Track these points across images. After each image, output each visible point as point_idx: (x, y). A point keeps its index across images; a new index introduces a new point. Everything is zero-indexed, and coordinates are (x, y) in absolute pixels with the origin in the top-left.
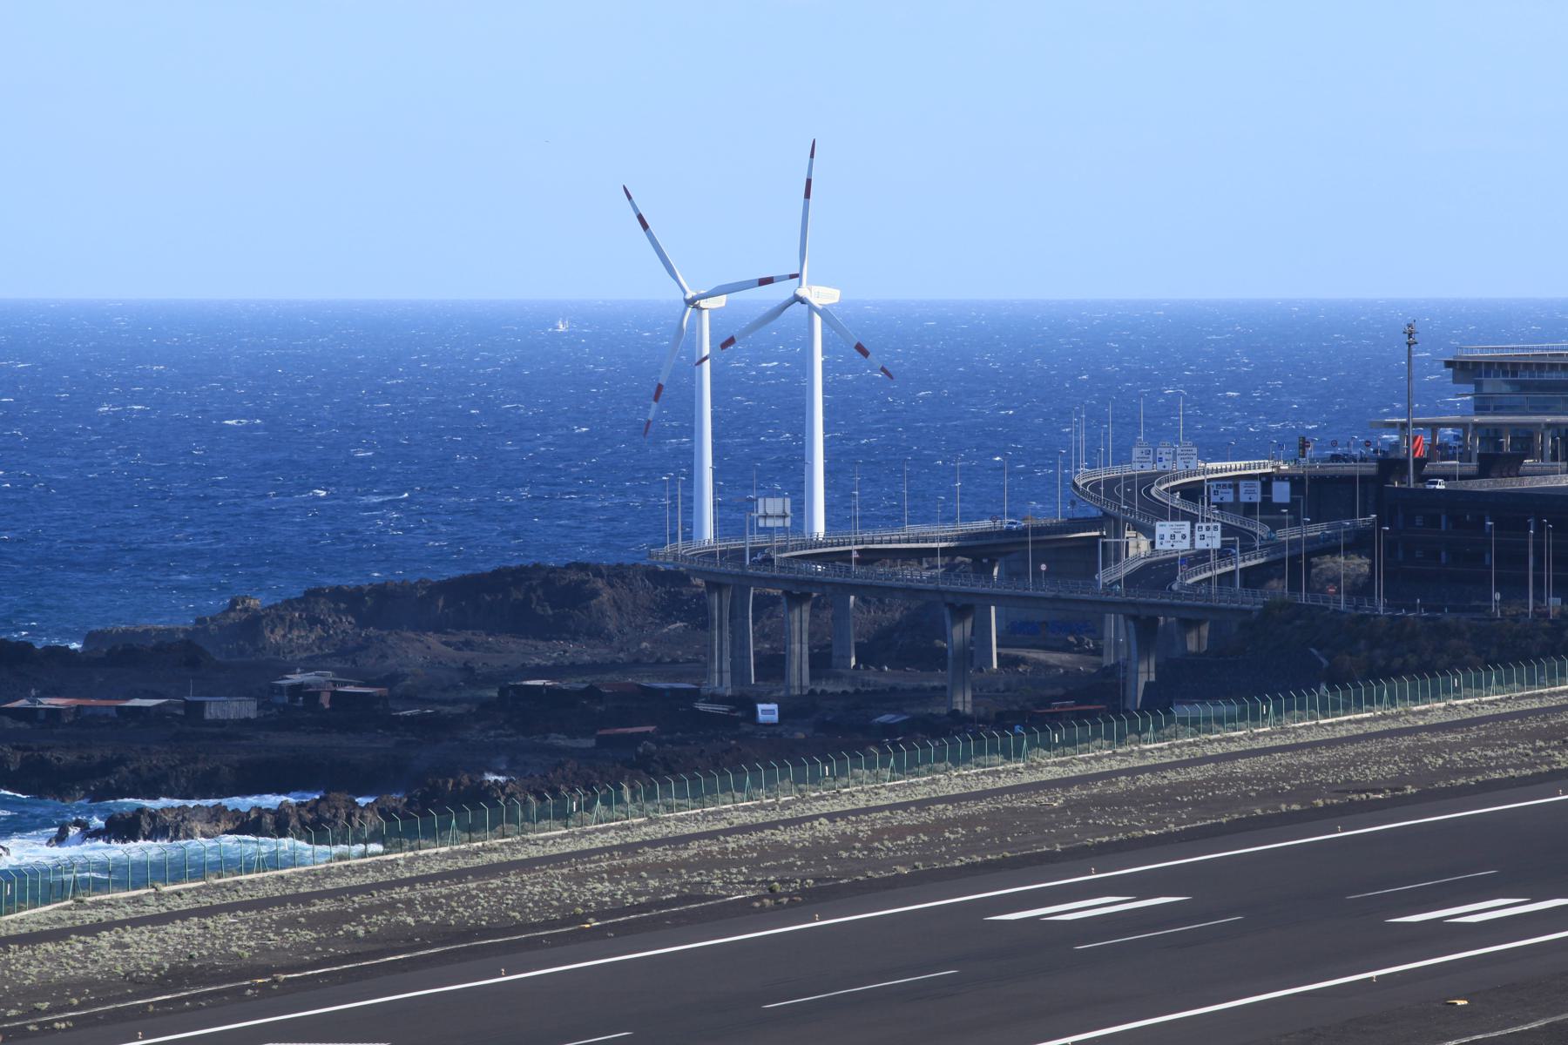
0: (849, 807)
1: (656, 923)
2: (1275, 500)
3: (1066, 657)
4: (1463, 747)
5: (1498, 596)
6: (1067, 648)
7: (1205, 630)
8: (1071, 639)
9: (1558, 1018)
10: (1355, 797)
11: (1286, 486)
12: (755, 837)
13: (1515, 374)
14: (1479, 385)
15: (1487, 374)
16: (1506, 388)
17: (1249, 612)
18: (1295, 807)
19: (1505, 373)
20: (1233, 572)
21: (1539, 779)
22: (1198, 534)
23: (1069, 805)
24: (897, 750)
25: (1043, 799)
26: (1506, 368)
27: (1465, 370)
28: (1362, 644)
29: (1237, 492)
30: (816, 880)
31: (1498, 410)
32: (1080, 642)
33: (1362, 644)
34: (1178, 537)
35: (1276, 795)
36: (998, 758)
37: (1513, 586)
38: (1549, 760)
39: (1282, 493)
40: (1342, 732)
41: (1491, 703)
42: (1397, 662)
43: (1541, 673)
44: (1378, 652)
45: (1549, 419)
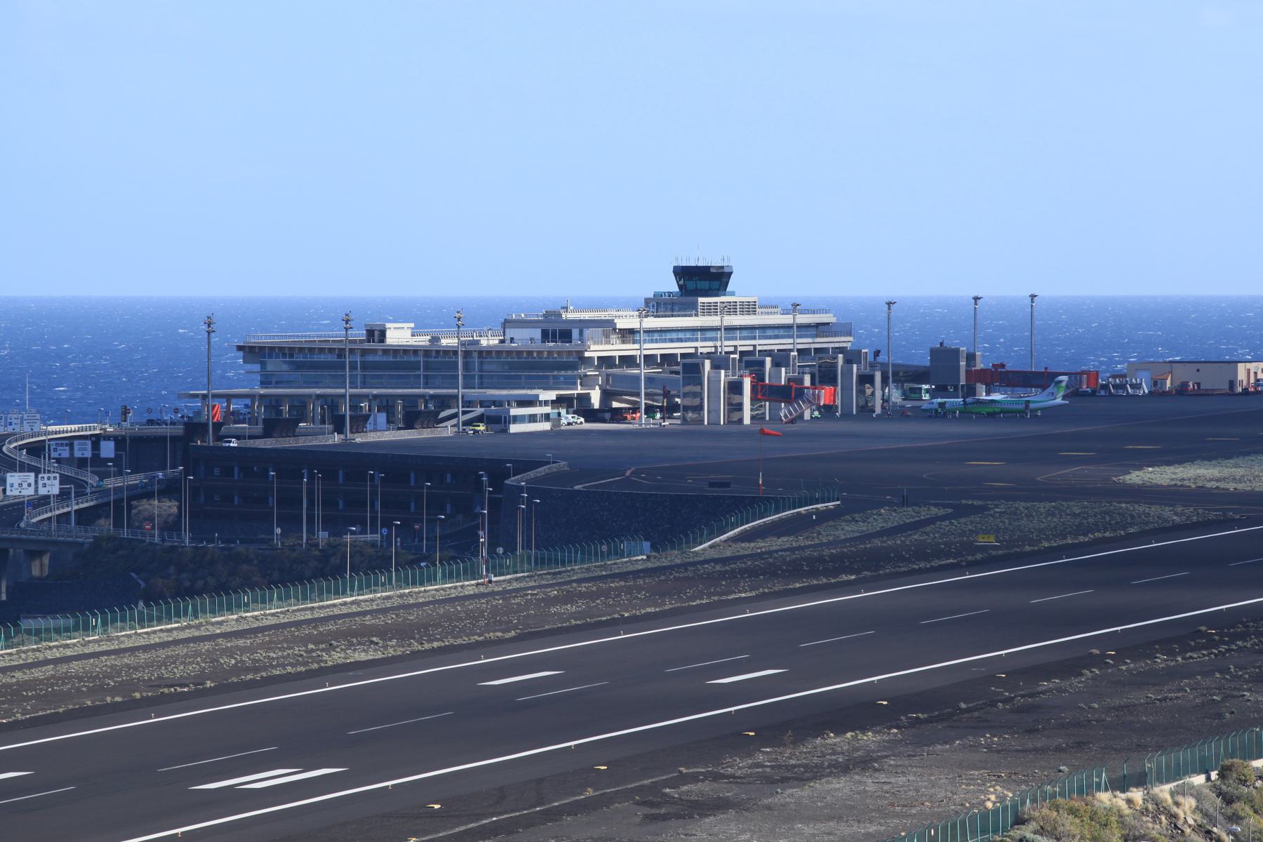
4: (251, 649)
5: (279, 531)
7: (46, 560)
11: (111, 444)
13: (291, 356)
15: (270, 356)
16: (285, 367)
17: (83, 544)
18: (118, 699)
19: (284, 355)
20: (69, 513)
21: (311, 674)
22: (40, 483)
27: (252, 352)
28: (172, 569)
29: (72, 449)
31: (278, 384)
33: (172, 569)
34: (25, 485)
35: (102, 689)
37: (291, 523)
39: (108, 450)
40: (155, 639)
41: (273, 615)
42: (200, 583)
44: (184, 575)
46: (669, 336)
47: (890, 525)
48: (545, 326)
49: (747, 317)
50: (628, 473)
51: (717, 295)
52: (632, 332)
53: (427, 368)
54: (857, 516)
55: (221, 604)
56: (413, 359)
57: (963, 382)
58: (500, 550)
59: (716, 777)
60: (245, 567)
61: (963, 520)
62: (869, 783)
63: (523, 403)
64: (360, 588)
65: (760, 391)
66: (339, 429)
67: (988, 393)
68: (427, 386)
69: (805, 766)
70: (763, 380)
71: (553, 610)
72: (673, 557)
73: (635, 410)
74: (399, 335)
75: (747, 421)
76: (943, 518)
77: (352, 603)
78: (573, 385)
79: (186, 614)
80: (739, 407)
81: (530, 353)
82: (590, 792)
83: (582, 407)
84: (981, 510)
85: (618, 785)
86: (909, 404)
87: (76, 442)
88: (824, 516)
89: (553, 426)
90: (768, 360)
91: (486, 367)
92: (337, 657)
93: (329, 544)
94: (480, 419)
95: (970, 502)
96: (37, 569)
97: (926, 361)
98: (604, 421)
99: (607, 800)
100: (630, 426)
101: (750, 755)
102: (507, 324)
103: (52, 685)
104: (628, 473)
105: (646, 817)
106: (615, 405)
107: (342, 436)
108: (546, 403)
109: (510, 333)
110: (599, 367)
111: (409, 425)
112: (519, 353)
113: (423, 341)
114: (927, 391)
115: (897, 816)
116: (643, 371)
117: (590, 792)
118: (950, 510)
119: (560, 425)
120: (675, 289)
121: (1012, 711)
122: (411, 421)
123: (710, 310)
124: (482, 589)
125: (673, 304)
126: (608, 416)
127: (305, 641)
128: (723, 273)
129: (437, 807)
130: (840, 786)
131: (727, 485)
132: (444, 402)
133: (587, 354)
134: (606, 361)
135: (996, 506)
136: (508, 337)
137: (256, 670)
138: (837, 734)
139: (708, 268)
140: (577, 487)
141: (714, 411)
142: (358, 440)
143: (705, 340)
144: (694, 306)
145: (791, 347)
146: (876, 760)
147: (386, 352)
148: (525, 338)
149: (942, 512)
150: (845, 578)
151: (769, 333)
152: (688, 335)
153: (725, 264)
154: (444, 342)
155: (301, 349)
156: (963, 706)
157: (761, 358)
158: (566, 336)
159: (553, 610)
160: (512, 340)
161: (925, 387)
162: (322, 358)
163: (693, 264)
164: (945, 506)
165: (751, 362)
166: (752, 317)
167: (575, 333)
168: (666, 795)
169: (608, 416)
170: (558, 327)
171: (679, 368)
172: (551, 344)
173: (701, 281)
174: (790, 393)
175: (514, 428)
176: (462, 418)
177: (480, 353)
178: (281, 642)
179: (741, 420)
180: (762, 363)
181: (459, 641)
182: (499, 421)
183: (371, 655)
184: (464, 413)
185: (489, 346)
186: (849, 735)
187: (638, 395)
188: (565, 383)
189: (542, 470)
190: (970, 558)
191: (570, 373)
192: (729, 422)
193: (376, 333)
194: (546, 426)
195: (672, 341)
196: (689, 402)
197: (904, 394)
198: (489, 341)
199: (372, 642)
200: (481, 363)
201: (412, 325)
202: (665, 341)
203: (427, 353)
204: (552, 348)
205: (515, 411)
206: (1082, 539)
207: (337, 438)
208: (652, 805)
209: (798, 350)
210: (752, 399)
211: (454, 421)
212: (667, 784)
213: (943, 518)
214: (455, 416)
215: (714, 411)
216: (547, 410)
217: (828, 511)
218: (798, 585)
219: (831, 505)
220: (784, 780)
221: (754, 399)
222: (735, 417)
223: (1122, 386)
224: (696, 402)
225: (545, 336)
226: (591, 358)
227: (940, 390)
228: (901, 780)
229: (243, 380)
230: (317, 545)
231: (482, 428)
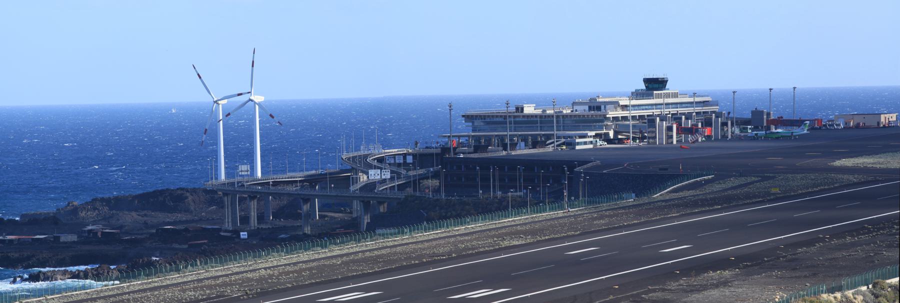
3: (341, 215)
4: (471, 241)
6: (341, 212)
14: (473, 123)
23: (343, 263)
27: (468, 118)
31: (479, 131)
35: (410, 258)
37: (486, 189)
39: (410, 159)
42: (449, 214)
52: (626, 106)
59: (664, 290)
65: (680, 130)
66: (505, 149)
68: (541, 130)
74: (529, 109)
75: (675, 142)
76: (757, 182)
80: (672, 137)
88: (708, 182)
92: (506, 243)
94: (563, 144)
97: (750, 116)
102: (574, 104)
106: (620, 137)
109: (576, 107)
110: (613, 121)
111: (534, 147)
113: (539, 112)
116: (631, 123)
120: (644, 88)
123: (659, 96)
127: (493, 237)
132: (548, 137)
141: (661, 139)
147: (524, 116)
148: (582, 110)
154: (548, 112)
158: (598, 108)
162: (497, 119)
163: (651, 77)
165: (676, 118)
167: (603, 107)
170: (595, 105)
173: (655, 84)
174: (692, 131)
175: (578, 147)
180: (681, 118)
182: (571, 145)
189: (589, 165)
194: (591, 146)
196: (650, 135)
198: (567, 111)
203: (541, 116)
204: (593, 113)
205: (578, 140)
207: (504, 153)
213: (757, 182)
214: (553, 143)
216: (591, 139)
220: (692, 291)
222: (670, 141)
223: (832, 125)
225: (590, 108)
231: (564, 147)
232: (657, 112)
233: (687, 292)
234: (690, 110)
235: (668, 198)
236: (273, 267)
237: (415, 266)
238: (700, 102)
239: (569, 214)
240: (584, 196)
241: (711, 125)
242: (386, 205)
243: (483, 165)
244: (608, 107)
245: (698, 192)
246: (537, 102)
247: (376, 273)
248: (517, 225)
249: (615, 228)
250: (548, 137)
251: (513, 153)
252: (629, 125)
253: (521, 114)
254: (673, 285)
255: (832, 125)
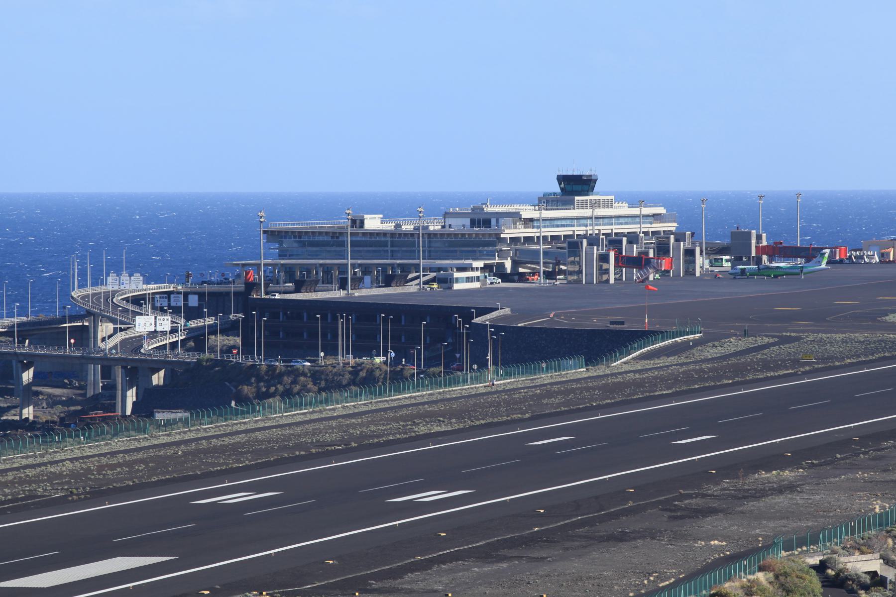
0: (80, 455)
1: (26, 507)
2: (190, 305)
3: (65, 391)
4: (361, 425)
5: (322, 354)
6: (64, 386)
7: (162, 373)
8: (66, 381)
9: (491, 540)
10: (329, 448)
11: (196, 297)
12: (38, 470)
13: (300, 237)
14: (281, 244)
15: (285, 238)
16: (295, 245)
17: (189, 363)
18: (303, 453)
19: (295, 237)
20: (177, 342)
21: (411, 439)
22: (158, 323)
23: (185, 454)
24: (90, 429)
25: (354, 421)
26: (296, 235)
27: (273, 235)
28: (253, 380)
29: (169, 300)
30: (91, 488)
31: (291, 257)
32: (71, 383)
33: (253, 380)
34: (148, 324)
35: (285, 448)
36: (132, 433)
37: (332, 350)
38: (411, 430)
39: (193, 301)
40: (299, 419)
41: (364, 404)
42: (273, 389)
43: (527, 369)
44: (262, 384)
45: (321, 262)
46: (557, 223)
47: (739, 349)
48: (473, 217)
49: (607, 210)
50: (552, 315)
51: (587, 195)
52: (532, 220)
53: (392, 246)
54: (716, 343)
55: (535, 369)
56: (383, 239)
57: (753, 254)
58: (475, 367)
59: (704, 496)
60: (302, 378)
61: (787, 346)
62: (798, 499)
63: (461, 269)
64: (404, 389)
65: (624, 262)
66: (343, 286)
67: (771, 261)
68: (392, 258)
69: (755, 489)
70: (621, 253)
71: (545, 401)
72: (600, 370)
73: (535, 273)
74: (373, 223)
75: (612, 281)
76: (774, 344)
77: (410, 397)
78: (493, 257)
79: (409, 389)
80: (607, 271)
81: (463, 235)
82: (631, 504)
83: (498, 271)
84: (797, 339)
85: (645, 500)
86: (717, 270)
87: (172, 296)
88: (697, 343)
89: (482, 285)
90: (625, 239)
91: (433, 245)
92: (422, 429)
93: (356, 363)
94: (433, 280)
95: (788, 334)
96: (158, 379)
97: (727, 241)
98: (513, 281)
99: (644, 508)
100: (533, 285)
101: (718, 484)
102: (446, 215)
103: (253, 446)
104: (552, 315)
105: (670, 517)
106: (521, 270)
107: (345, 292)
108: (477, 269)
109: (450, 221)
110: (509, 245)
111: (388, 285)
112: (456, 235)
113: (390, 226)
114: (727, 261)
115: (822, 517)
116: (542, 247)
117: (631, 504)
118: (777, 339)
119: (486, 284)
120: (558, 190)
121: (870, 459)
122: (388, 281)
123: (583, 205)
124: (489, 389)
125: (557, 201)
126: (516, 278)
127: (396, 420)
128: (591, 180)
129: (207, 592)
130: (782, 501)
131: (622, 323)
132: (406, 269)
133: (502, 236)
134: (515, 240)
135: (807, 337)
136: (447, 224)
137: (378, 437)
138: (767, 472)
139: (581, 176)
140: (520, 325)
141: (589, 275)
142: (356, 294)
143: (580, 225)
144: (572, 202)
145: (638, 230)
146: (798, 486)
147: (364, 234)
148: (459, 225)
149: (771, 340)
150: (726, 382)
151: (622, 220)
152: (568, 222)
153: (592, 173)
154: (404, 228)
155: (306, 233)
156: (839, 456)
157: (579, 240)
158: (487, 223)
159: (545, 401)
160: (450, 226)
161: (725, 258)
162: (321, 239)
163: (570, 173)
164: (773, 337)
165: (614, 241)
166: (610, 210)
167: (493, 221)
168: (676, 505)
169: (516, 278)
170: (482, 217)
171: (564, 245)
172: (477, 229)
173: (576, 185)
174: (641, 262)
175: (456, 286)
176: (423, 279)
177: (429, 235)
178: (381, 420)
179: (608, 281)
180: (621, 242)
181: (496, 420)
182: (446, 282)
183: (443, 428)
184: (424, 276)
185: (435, 230)
186: (774, 472)
187: (538, 263)
188: (488, 255)
189: (494, 314)
190: (802, 369)
191: (490, 248)
192: (600, 282)
193: (358, 222)
194: (476, 285)
195: (558, 226)
196: (571, 268)
197: (710, 262)
198: (435, 227)
199: (439, 421)
200: (430, 242)
201: (381, 216)
202: (553, 226)
203: (392, 235)
204: (477, 234)
205: (457, 275)
206: (871, 357)
207: (341, 294)
208: (671, 511)
209: (643, 232)
210: (615, 267)
211: (417, 281)
212: (674, 499)
213: (774, 344)
214: (418, 277)
215: (589, 272)
216: (478, 274)
217: (694, 341)
218: (697, 386)
219: (696, 336)
220: (745, 497)
221: (616, 266)
222: (605, 277)
223: (861, 257)
224: (577, 268)
225: (473, 223)
226: (505, 239)
227: (738, 260)
228: (817, 497)
229: (267, 257)
230: (348, 364)
231: (435, 286)
232: (579, 230)
233: (739, 498)
234: (633, 228)
235: (639, 367)
236: (83, 458)
237: (301, 458)
238: (647, 216)
239: (494, 389)
240: (496, 363)
241: (667, 252)
242: (162, 373)
243: (299, 309)
244: (502, 221)
245: (683, 359)
246: (387, 210)
247: (247, 468)
248: (423, 404)
249: (579, 410)
250: (406, 269)
251: (357, 293)
252: (537, 252)
253: (360, 230)
254: (714, 489)
255: (861, 257)
